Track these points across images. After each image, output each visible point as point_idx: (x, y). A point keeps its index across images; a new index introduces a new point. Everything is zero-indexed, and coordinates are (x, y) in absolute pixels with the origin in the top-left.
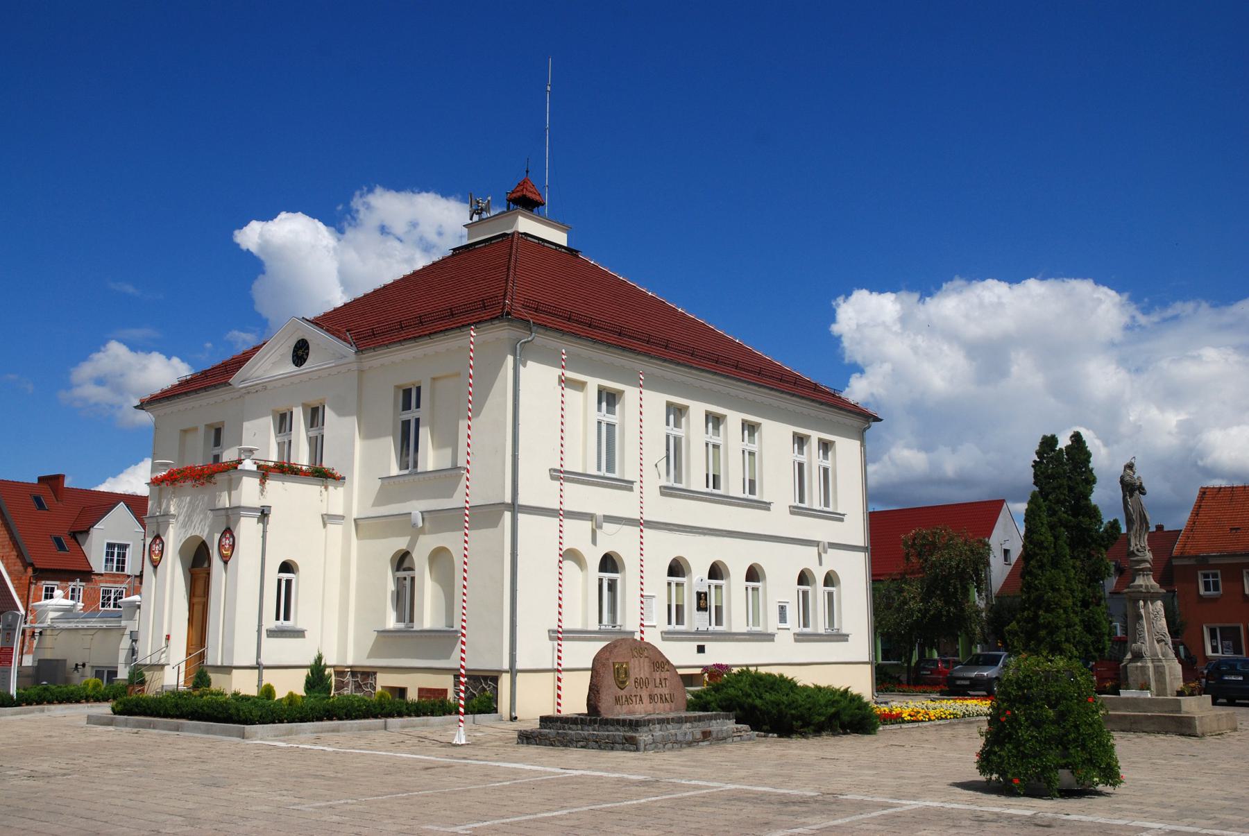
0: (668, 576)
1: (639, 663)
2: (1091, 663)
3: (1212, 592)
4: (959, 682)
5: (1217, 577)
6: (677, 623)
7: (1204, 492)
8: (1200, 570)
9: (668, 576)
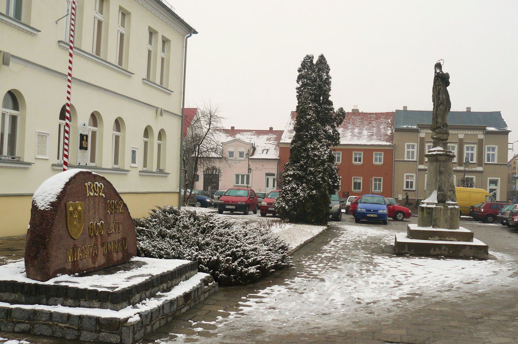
0: (60, 119)
1: (94, 203)
2: (86, 184)
3: (358, 162)
4: (272, 215)
5: (381, 156)
6: (411, 188)
7: (358, 110)
8: (354, 151)
9: (60, 119)
